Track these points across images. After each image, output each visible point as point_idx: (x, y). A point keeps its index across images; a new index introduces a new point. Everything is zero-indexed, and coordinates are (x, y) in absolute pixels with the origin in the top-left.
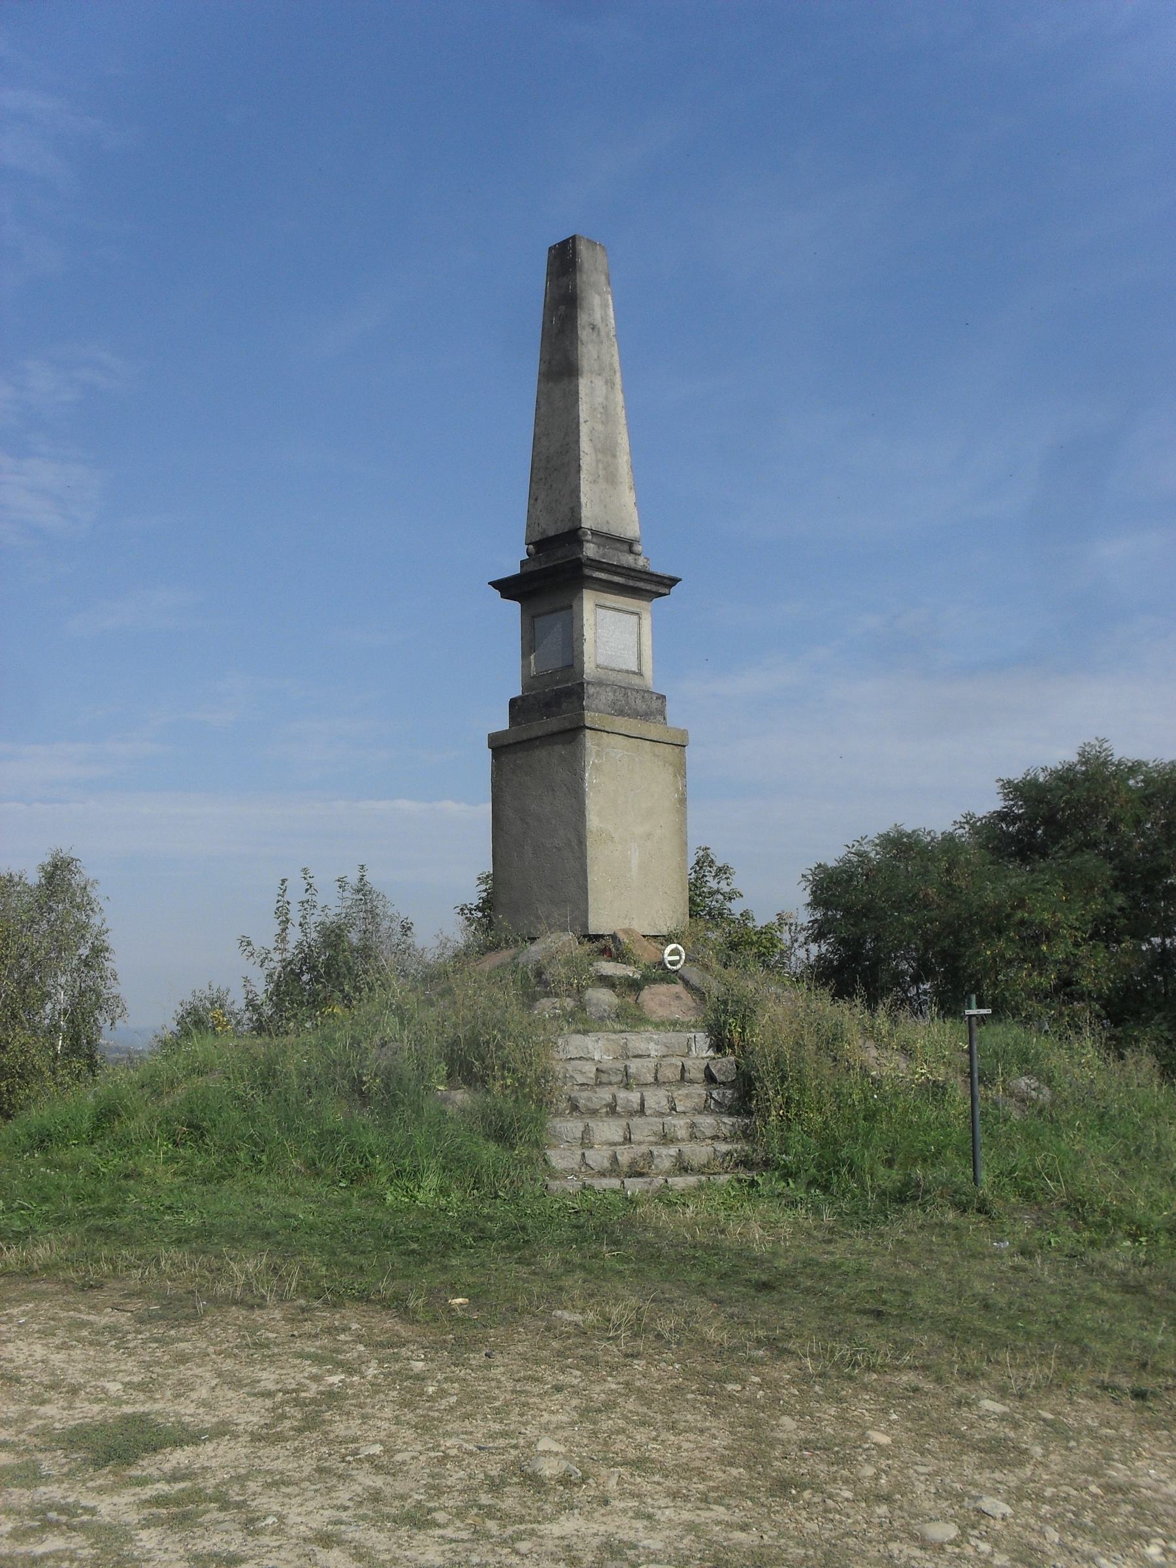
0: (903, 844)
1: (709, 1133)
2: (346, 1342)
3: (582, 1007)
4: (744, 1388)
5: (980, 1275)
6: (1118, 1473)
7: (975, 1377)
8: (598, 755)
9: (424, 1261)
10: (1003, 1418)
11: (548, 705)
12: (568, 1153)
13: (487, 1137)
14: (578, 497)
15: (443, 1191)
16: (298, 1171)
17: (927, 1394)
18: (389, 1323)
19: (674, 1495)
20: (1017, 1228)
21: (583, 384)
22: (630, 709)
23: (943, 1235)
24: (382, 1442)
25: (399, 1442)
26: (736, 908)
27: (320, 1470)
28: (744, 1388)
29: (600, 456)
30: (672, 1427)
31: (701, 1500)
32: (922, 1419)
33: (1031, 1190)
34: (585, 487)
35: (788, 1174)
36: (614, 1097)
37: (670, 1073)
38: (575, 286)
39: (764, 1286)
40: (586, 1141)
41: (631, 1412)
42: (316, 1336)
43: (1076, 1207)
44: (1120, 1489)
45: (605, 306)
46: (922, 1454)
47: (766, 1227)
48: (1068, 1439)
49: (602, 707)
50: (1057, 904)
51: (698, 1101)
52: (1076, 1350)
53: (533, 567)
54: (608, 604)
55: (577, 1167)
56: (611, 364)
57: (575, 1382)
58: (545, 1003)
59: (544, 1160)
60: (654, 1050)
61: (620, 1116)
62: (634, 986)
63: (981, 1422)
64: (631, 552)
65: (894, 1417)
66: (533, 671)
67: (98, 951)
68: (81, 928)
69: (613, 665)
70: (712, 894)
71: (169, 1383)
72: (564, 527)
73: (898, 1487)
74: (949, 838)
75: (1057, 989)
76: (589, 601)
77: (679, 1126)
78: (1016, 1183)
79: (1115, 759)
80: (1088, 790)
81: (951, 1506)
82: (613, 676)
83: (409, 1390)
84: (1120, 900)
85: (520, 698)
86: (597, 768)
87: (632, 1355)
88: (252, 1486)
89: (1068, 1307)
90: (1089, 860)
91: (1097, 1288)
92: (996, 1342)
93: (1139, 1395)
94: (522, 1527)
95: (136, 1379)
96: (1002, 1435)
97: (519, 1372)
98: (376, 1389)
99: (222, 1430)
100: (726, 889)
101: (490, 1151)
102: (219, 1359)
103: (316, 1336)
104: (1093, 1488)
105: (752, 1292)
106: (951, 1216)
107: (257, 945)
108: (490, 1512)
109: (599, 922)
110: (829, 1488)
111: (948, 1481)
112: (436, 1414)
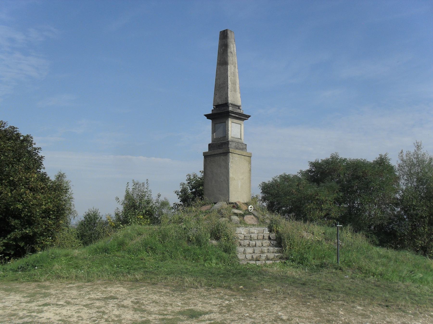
1: (272, 251)
10: (362, 310)
11: (219, 146)
21: (229, 67)
34: (229, 93)
35: (293, 261)
37: (261, 237)
38: (227, 42)
40: (244, 252)
50: (326, 194)
53: (215, 112)
60: (256, 232)
61: (250, 247)
62: (243, 216)
64: (239, 109)
66: (215, 138)
74: (295, 176)
75: (325, 216)
76: (230, 121)
77: (265, 249)
78: (346, 264)
79: (339, 158)
80: (333, 166)
82: (235, 140)
84: (341, 194)
90: (333, 184)
92: (356, 296)
93: (387, 306)
101: (224, 254)
106: (334, 270)
109: (233, 199)
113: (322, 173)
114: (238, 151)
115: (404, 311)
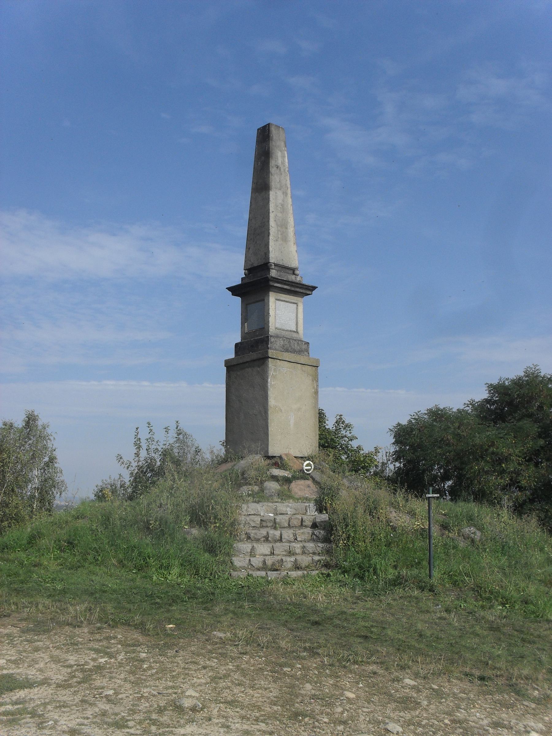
0: (439, 414)
2: (114, 644)
3: (262, 490)
4: (292, 670)
5: (422, 620)
6: (460, 715)
7: (404, 669)
8: (275, 370)
9: (159, 608)
10: (413, 687)
11: (252, 346)
12: (242, 559)
13: (205, 551)
14: (268, 248)
15: (181, 575)
16: (114, 565)
17: (380, 675)
18: (136, 635)
19: (243, 717)
20: (446, 599)
21: (272, 194)
22: (291, 349)
23: (410, 602)
24: (115, 689)
25: (123, 690)
26: (354, 444)
27: (82, 701)
28: (292, 670)
29: (279, 228)
30: (252, 687)
31: (255, 720)
32: (374, 687)
33: (456, 581)
34: (271, 243)
36: (268, 533)
37: (296, 522)
39: (316, 623)
40: (252, 553)
41: (235, 679)
42: (100, 640)
43: (478, 590)
44: (459, 722)
45: (283, 157)
46: (368, 703)
47: (326, 596)
48: (442, 698)
49: (277, 348)
51: (307, 537)
52: (456, 657)
53: (247, 281)
54: (282, 299)
55: (246, 566)
56: (286, 185)
57: (214, 664)
58: (245, 488)
59: (231, 562)
60: (289, 511)
61: (270, 542)
62: (288, 481)
63: (402, 690)
64: (294, 274)
65: (361, 685)
66: (246, 331)
67: (52, 460)
68: (45, 447)
69: (284, 328)
70: (343, 437)
71: (28, 660)
72: (261, 262)
73: (352, 718)
76: (272, 297)
77: (297, 547)
78: (450, 577)
79: (542, 374)
81: (374, 727)
82: (283, 333)
83: (136, 667)
84: (541, 442)
85: (240, 343)
86: (274, 377)
87: (243, 653)
88: (49, 707)
89: (460, 637)
91: (477, 628)
93: (482, 678)
94: (167, 730)
95: (13, 658)
96: (410, 695)
97: (188, 659)
98: (121, 665)
99: (45, 682)
100: (349, 435)
102: (53, 650)
103: (100, 640)
104: (446, 721)
105: (309, 625)
107: (125, 459)
108: (154, 722)
109: (274, 449)
110: (318, 717)
111: (376, 715)
112: (144, 677)
113: (510, 404)
114: (287, 356)
115: (518, 693)
